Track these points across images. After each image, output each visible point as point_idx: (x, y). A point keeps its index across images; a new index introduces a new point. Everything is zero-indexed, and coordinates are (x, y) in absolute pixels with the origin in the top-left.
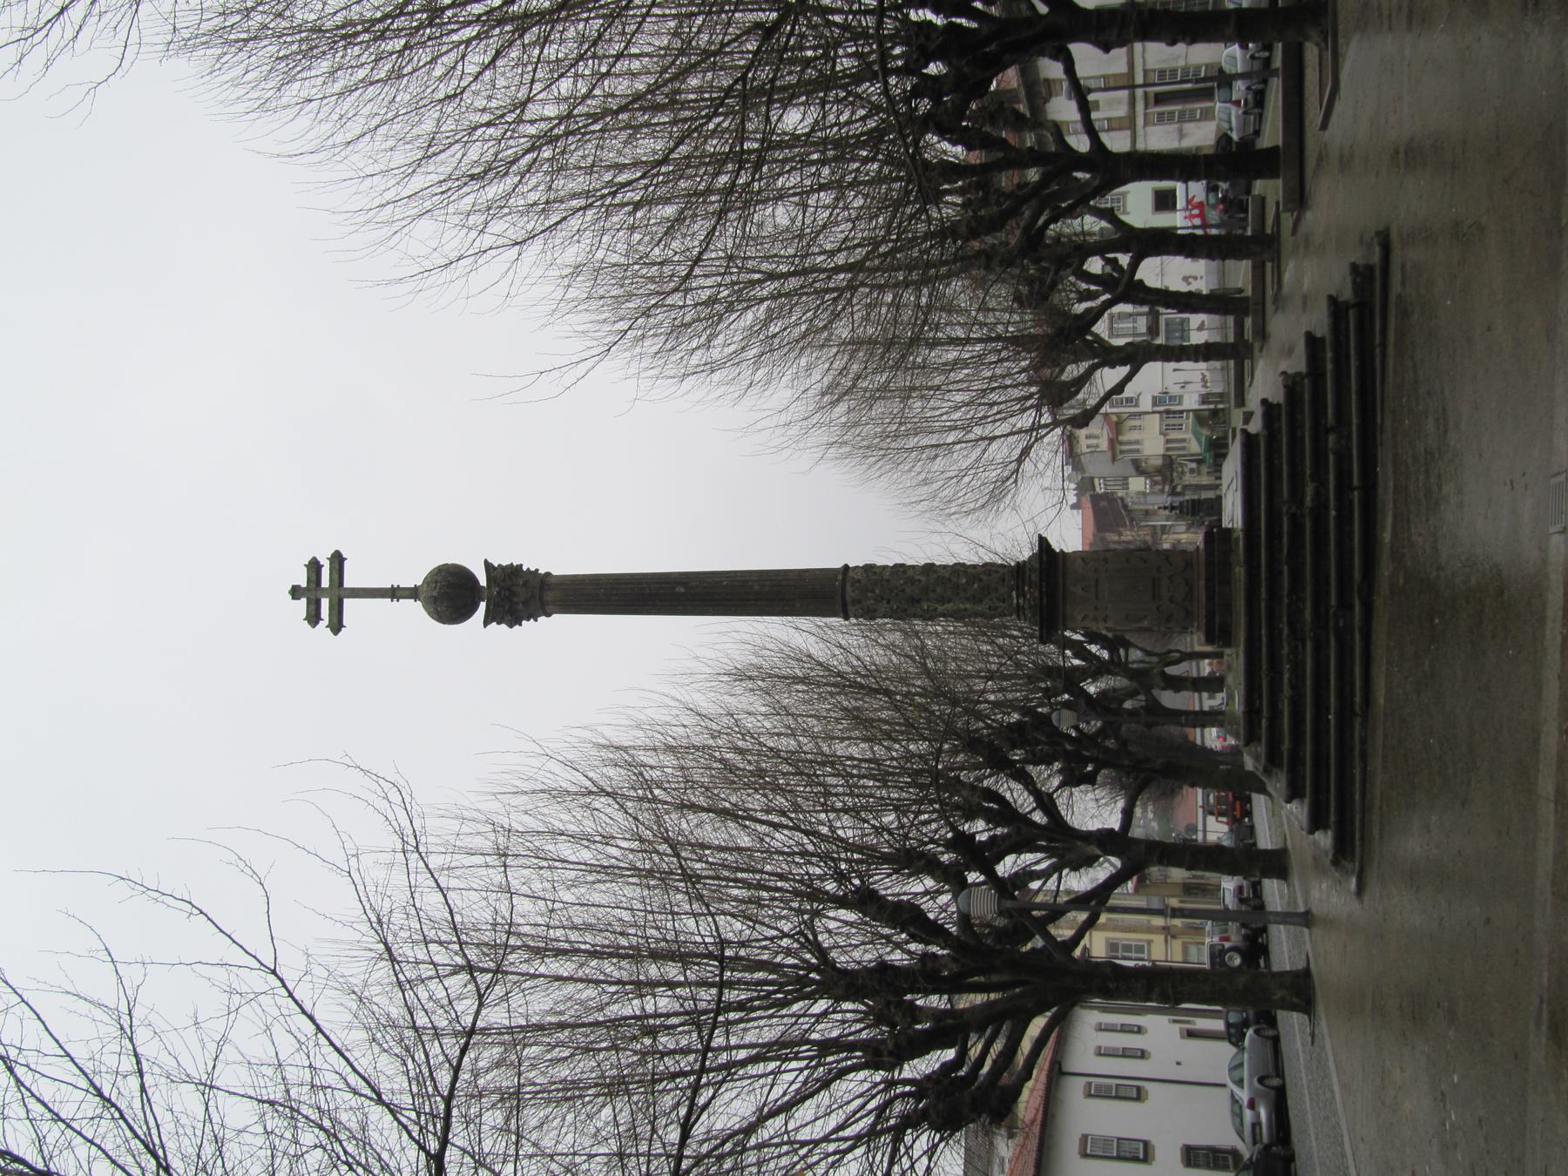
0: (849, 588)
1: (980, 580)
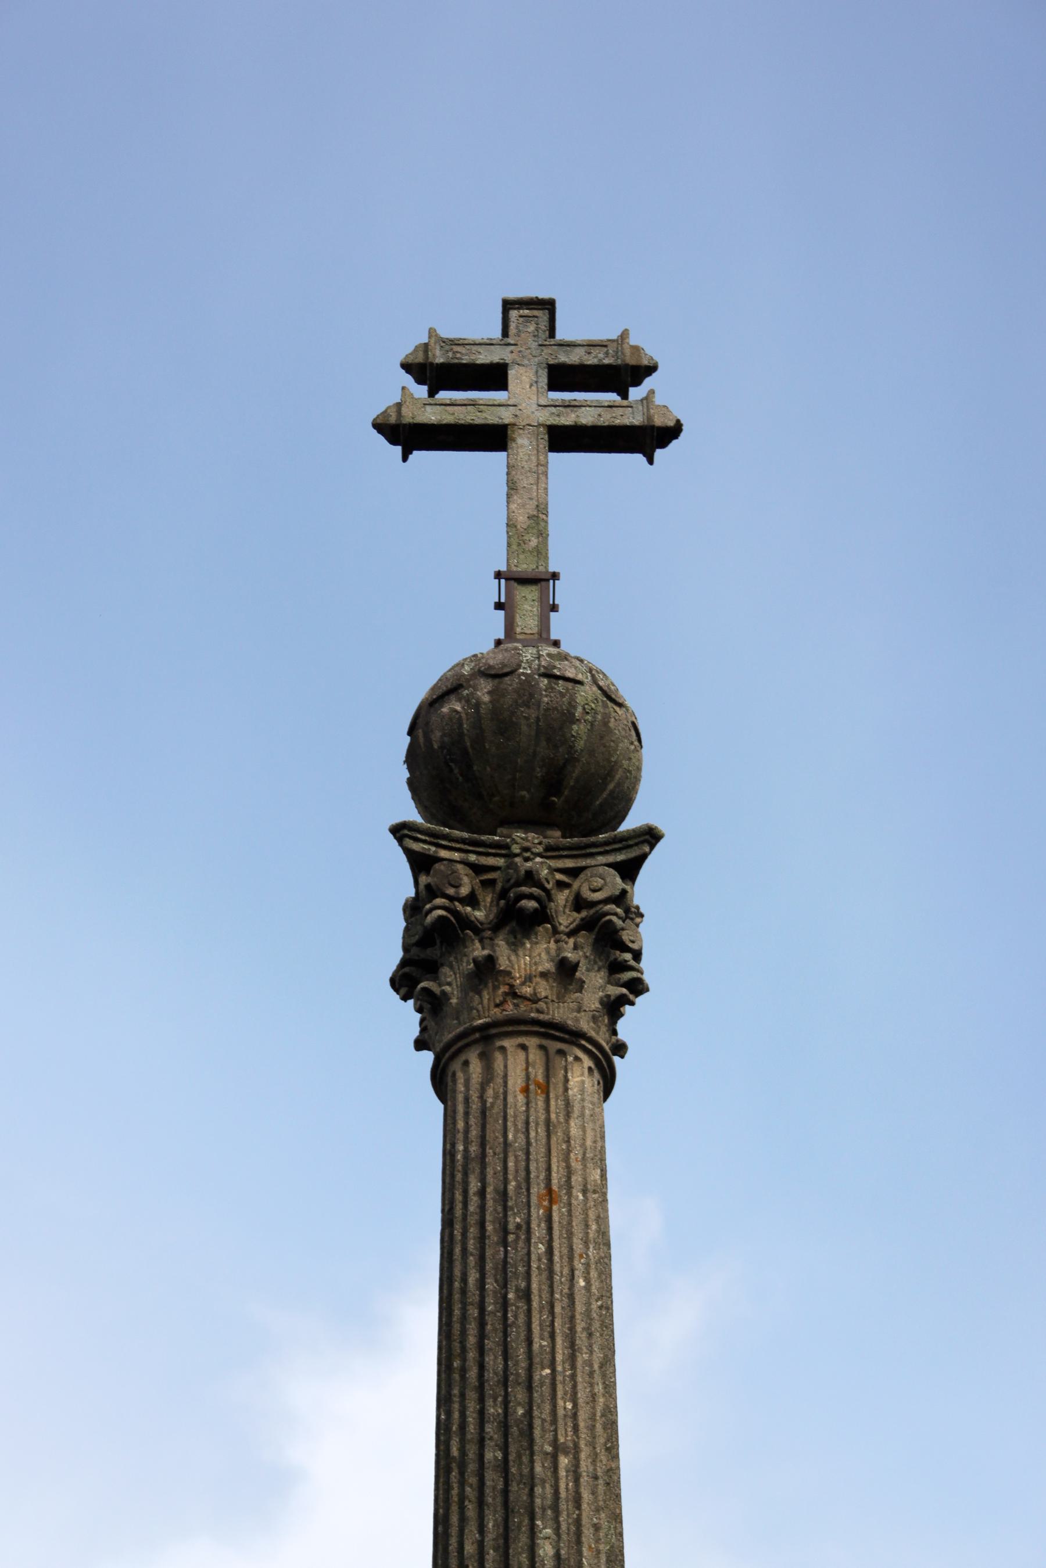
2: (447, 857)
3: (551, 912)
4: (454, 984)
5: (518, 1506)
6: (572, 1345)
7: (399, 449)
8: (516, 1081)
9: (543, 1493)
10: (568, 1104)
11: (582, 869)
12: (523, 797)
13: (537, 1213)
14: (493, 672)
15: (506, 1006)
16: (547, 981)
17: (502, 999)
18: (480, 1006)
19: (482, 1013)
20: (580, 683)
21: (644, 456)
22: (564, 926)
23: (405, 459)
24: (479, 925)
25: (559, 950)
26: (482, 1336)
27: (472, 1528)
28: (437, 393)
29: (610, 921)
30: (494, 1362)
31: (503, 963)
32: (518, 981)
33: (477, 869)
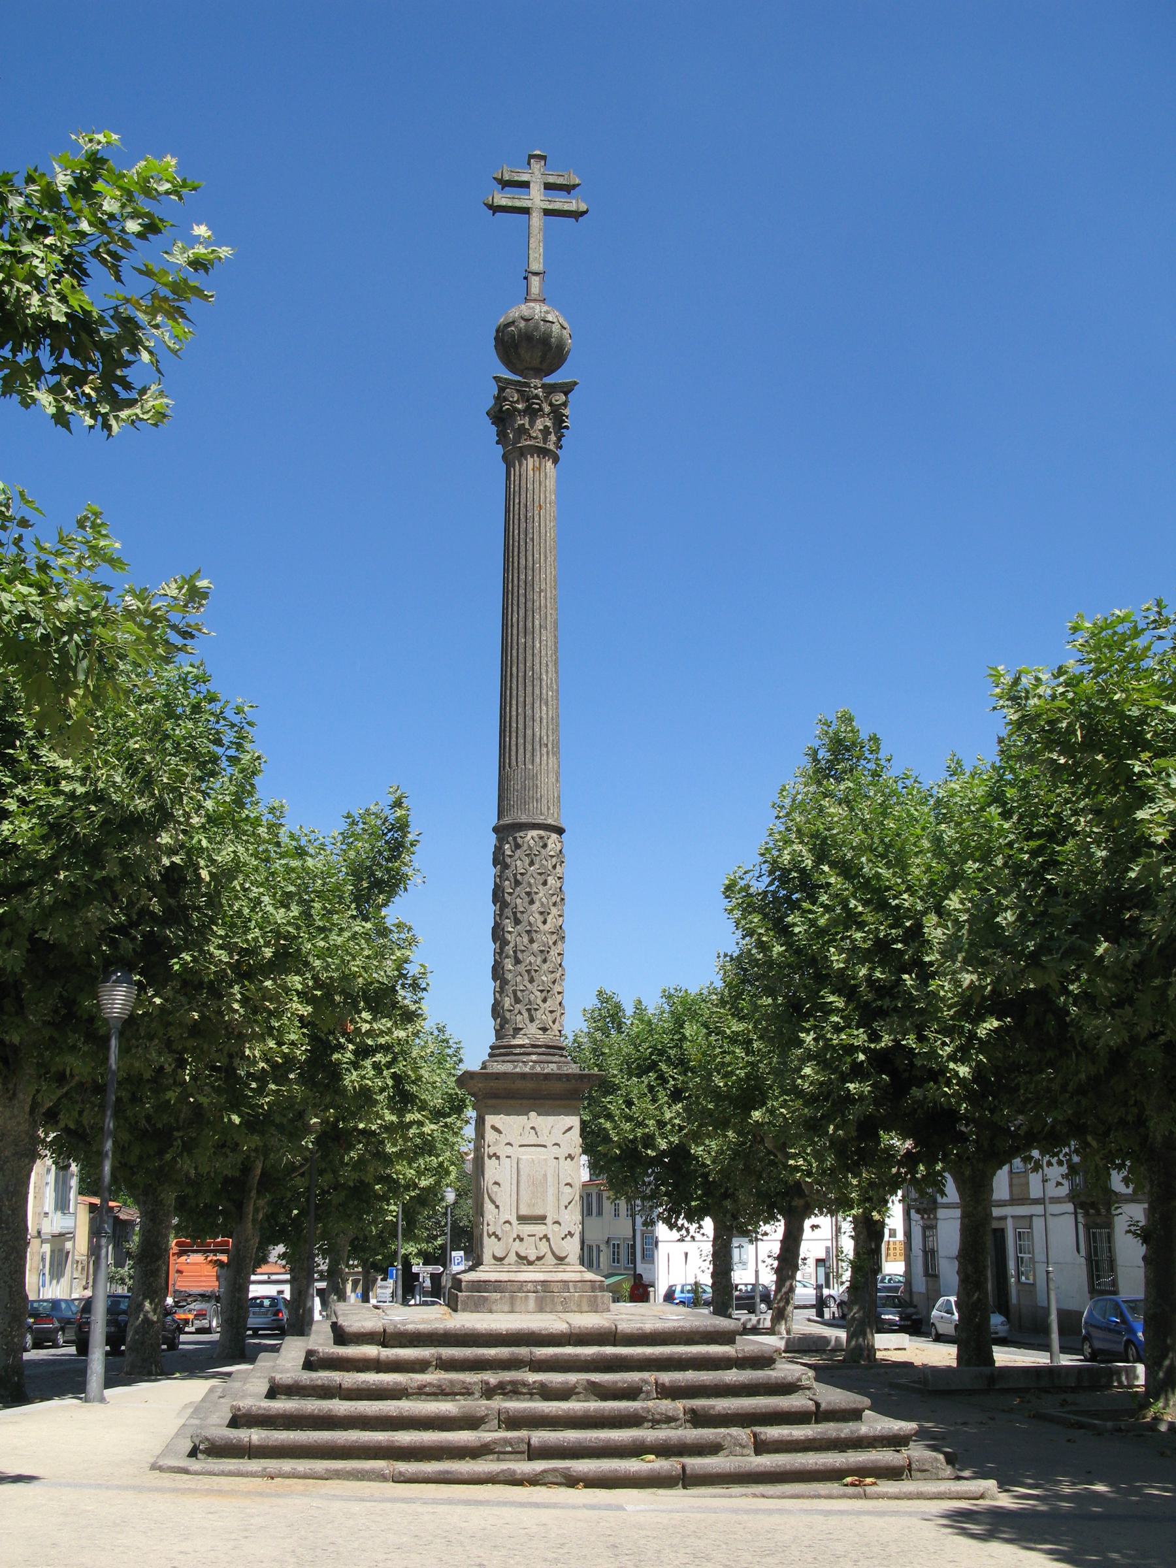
0: (535, 833)
1: (544, 1000)
6: (546, 556)
8: (530, 466)
9: (537, 604)
10: (546, 474)
13: (536, 512)
20: (553, 323)
26: (519, 552)
27: (515, 614)
30: (523, 562)
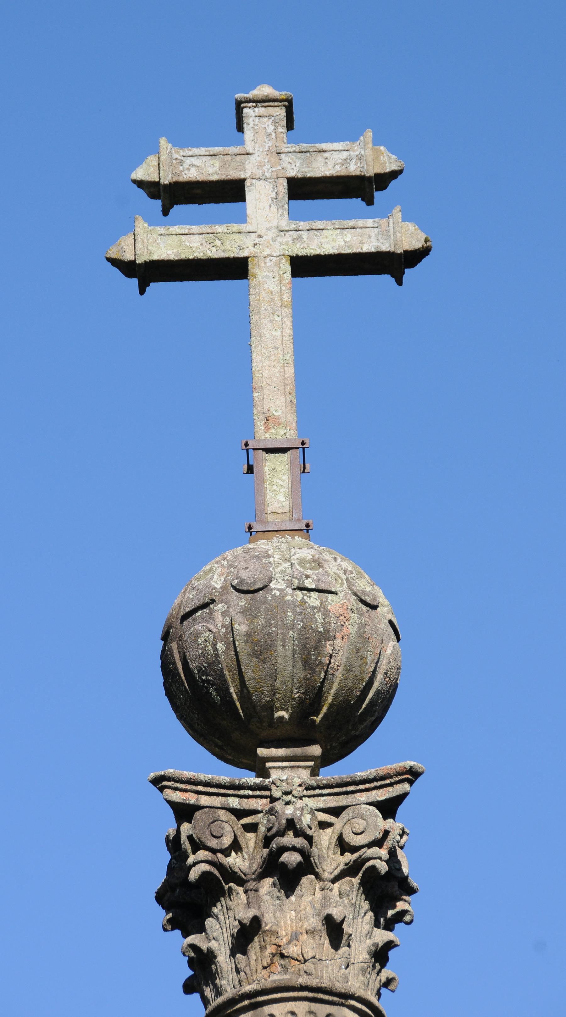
2: (208, 805)
3: (314, 860)
4: (221, 939)
5: (296, 578)
7: (135, 281)
11: (343, 808)
12: (282, 718)
14: (245, 588)
15: (273, 968)
16: (314, 938)
17: (269, 961)
18: (248, 968)
19: (249, 976)
21: (392, 276)
22: (328, 872)
23: (142, 291)
24: (243, 876)
25: (325, 901)
28: (197, 852)
29: (373, 868)
31: (268, 922)
32: (284, 940)
33: (239, 814)
